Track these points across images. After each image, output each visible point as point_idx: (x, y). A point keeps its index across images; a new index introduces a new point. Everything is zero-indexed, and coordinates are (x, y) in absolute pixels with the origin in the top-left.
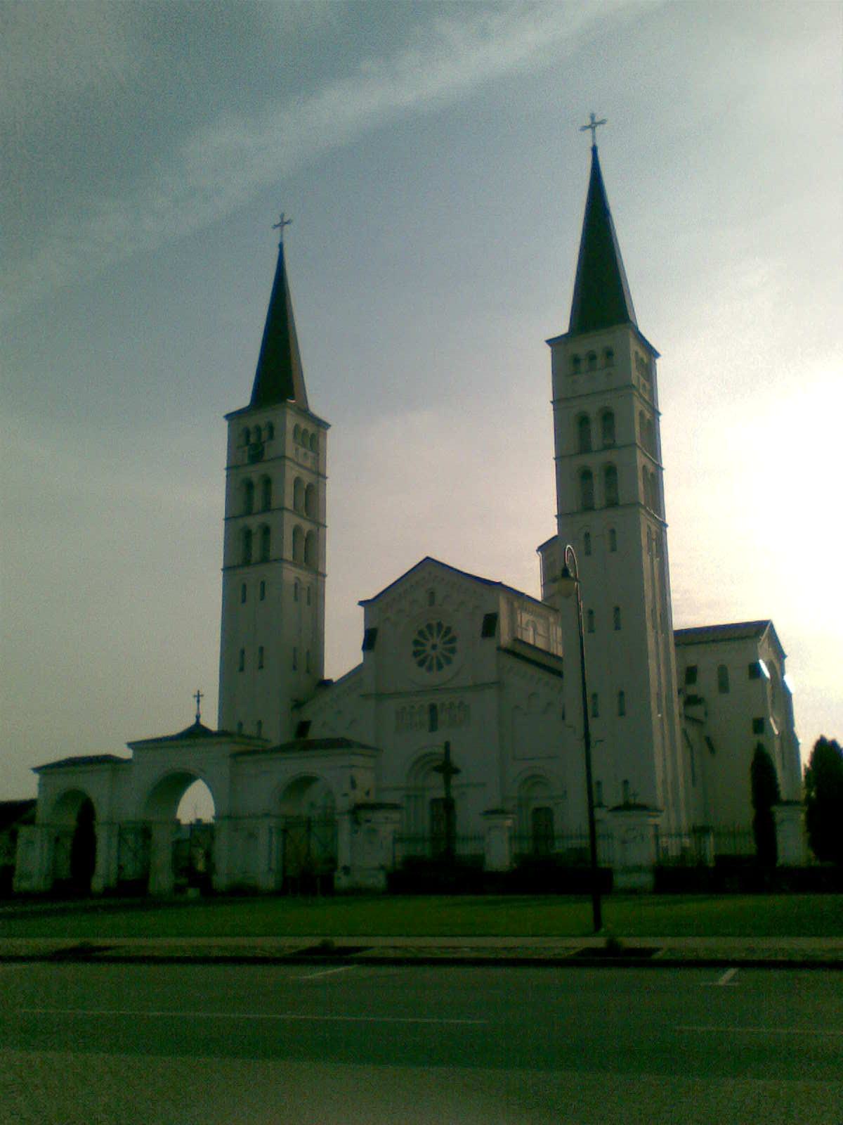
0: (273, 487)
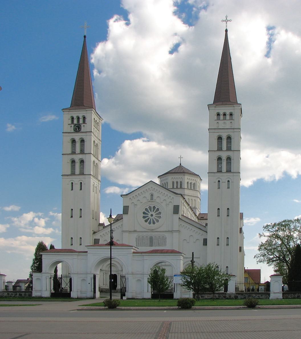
0: (86, 119)
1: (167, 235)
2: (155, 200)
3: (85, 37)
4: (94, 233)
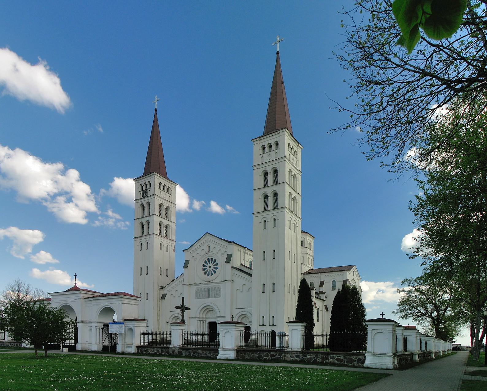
1: (221, 285)
2: (212, 251)
3: (278, 53)
4: (162, 288)
